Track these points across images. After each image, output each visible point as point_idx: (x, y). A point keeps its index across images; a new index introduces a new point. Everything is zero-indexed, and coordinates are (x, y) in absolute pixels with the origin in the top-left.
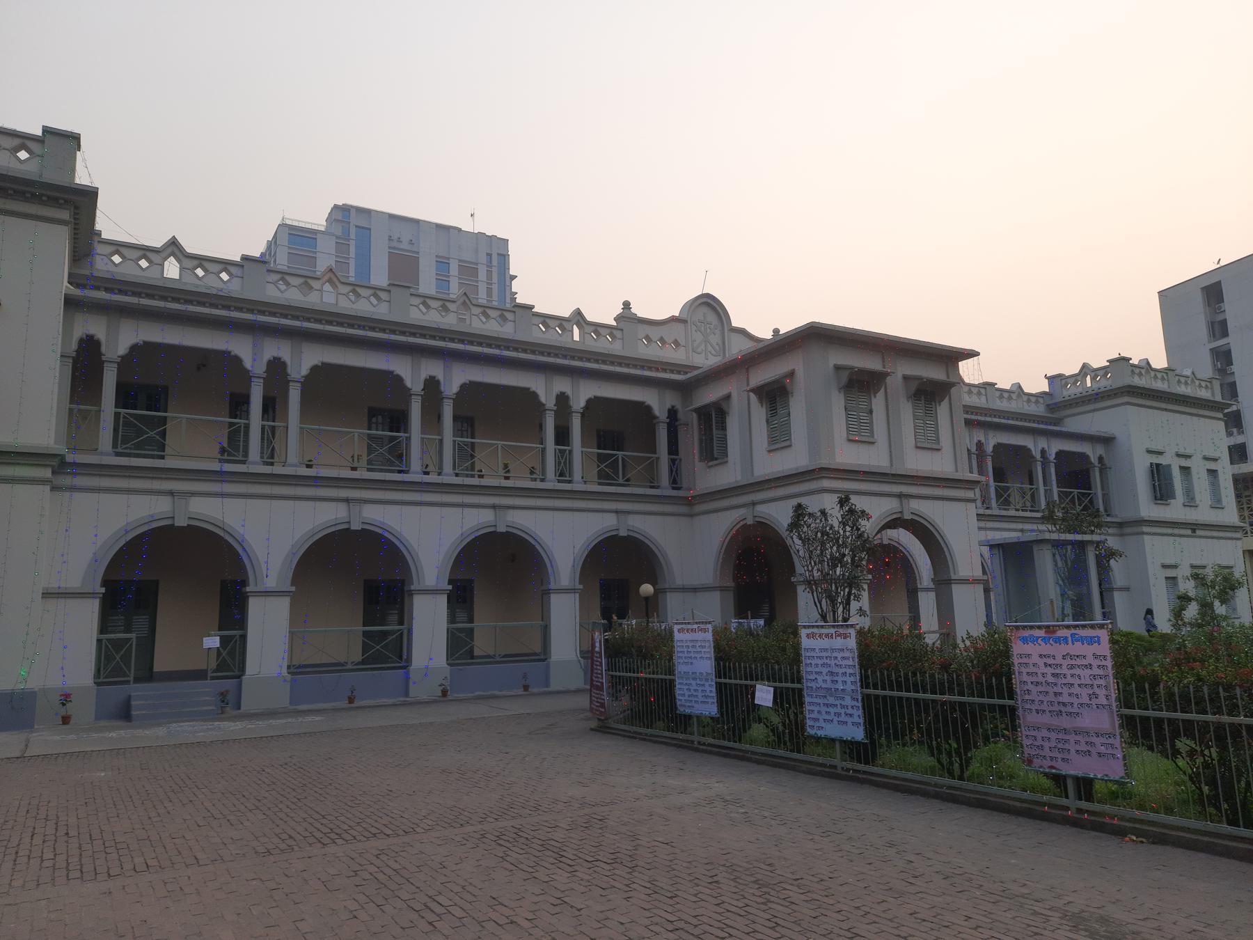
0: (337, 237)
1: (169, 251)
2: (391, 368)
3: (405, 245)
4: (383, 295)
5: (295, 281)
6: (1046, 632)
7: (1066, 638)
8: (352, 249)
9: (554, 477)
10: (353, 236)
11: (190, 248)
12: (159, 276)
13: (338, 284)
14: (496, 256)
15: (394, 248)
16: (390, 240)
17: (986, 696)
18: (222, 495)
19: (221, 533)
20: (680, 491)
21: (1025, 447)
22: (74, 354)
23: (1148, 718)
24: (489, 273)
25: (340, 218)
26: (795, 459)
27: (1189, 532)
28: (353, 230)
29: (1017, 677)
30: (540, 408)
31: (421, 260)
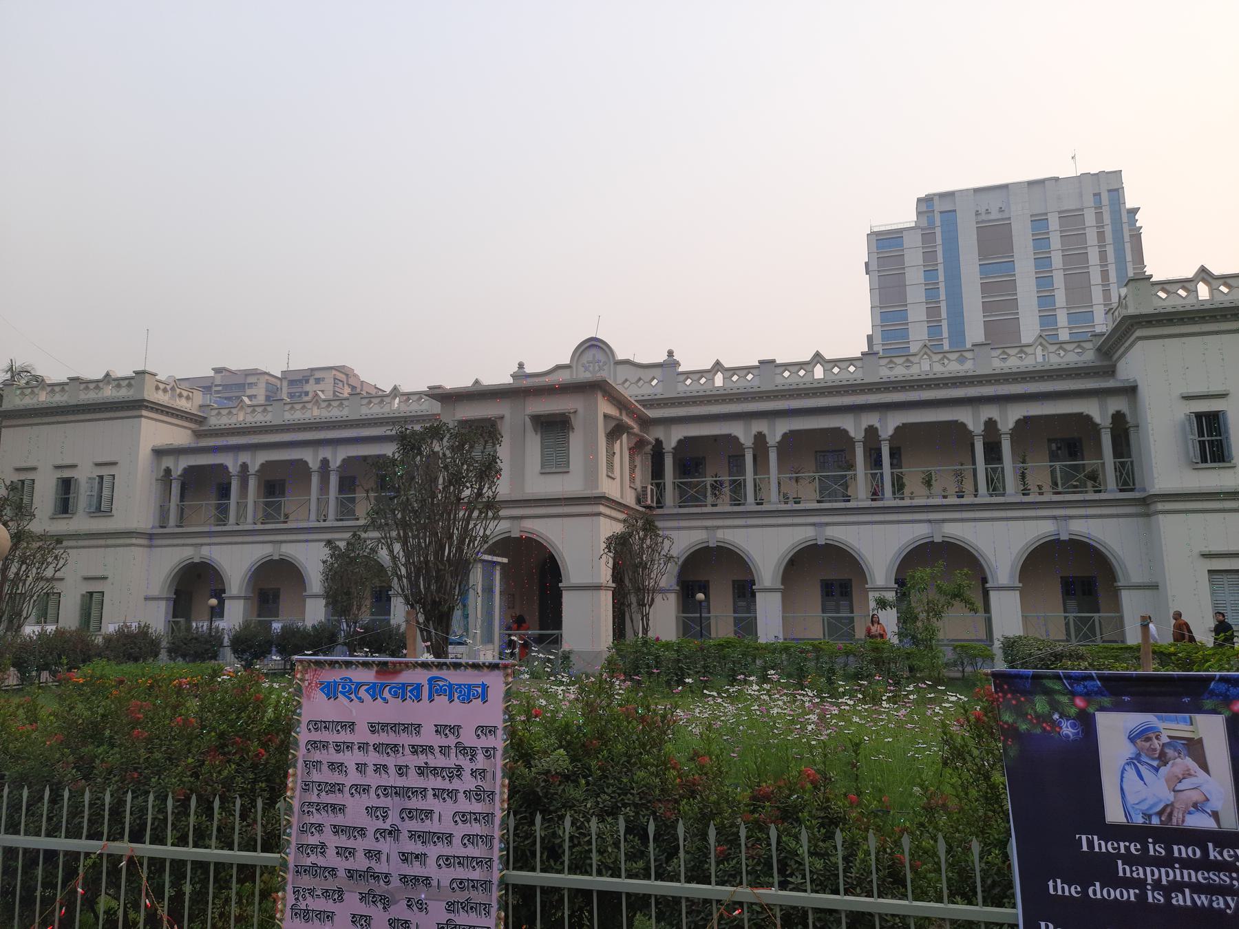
0: (922, 229)
2: (955, 419)
3: (995, 215)
6: (377, 672)
7: (419, 687)
8: (939, 240)
10: (938, 223)
11: (405, 388)
12: (711, 387)
14: (1106, 193)
15: (983, 221)
16: (976, 215)
17: (713, 879)
18: (1087, 517)
21: (222, 465)
23: (586, 894)
24: (1099, 215)
25: (925, 209)
28: (938, 217)
29: (299, 772)
30: (851, 442)
31: (1014, 227)
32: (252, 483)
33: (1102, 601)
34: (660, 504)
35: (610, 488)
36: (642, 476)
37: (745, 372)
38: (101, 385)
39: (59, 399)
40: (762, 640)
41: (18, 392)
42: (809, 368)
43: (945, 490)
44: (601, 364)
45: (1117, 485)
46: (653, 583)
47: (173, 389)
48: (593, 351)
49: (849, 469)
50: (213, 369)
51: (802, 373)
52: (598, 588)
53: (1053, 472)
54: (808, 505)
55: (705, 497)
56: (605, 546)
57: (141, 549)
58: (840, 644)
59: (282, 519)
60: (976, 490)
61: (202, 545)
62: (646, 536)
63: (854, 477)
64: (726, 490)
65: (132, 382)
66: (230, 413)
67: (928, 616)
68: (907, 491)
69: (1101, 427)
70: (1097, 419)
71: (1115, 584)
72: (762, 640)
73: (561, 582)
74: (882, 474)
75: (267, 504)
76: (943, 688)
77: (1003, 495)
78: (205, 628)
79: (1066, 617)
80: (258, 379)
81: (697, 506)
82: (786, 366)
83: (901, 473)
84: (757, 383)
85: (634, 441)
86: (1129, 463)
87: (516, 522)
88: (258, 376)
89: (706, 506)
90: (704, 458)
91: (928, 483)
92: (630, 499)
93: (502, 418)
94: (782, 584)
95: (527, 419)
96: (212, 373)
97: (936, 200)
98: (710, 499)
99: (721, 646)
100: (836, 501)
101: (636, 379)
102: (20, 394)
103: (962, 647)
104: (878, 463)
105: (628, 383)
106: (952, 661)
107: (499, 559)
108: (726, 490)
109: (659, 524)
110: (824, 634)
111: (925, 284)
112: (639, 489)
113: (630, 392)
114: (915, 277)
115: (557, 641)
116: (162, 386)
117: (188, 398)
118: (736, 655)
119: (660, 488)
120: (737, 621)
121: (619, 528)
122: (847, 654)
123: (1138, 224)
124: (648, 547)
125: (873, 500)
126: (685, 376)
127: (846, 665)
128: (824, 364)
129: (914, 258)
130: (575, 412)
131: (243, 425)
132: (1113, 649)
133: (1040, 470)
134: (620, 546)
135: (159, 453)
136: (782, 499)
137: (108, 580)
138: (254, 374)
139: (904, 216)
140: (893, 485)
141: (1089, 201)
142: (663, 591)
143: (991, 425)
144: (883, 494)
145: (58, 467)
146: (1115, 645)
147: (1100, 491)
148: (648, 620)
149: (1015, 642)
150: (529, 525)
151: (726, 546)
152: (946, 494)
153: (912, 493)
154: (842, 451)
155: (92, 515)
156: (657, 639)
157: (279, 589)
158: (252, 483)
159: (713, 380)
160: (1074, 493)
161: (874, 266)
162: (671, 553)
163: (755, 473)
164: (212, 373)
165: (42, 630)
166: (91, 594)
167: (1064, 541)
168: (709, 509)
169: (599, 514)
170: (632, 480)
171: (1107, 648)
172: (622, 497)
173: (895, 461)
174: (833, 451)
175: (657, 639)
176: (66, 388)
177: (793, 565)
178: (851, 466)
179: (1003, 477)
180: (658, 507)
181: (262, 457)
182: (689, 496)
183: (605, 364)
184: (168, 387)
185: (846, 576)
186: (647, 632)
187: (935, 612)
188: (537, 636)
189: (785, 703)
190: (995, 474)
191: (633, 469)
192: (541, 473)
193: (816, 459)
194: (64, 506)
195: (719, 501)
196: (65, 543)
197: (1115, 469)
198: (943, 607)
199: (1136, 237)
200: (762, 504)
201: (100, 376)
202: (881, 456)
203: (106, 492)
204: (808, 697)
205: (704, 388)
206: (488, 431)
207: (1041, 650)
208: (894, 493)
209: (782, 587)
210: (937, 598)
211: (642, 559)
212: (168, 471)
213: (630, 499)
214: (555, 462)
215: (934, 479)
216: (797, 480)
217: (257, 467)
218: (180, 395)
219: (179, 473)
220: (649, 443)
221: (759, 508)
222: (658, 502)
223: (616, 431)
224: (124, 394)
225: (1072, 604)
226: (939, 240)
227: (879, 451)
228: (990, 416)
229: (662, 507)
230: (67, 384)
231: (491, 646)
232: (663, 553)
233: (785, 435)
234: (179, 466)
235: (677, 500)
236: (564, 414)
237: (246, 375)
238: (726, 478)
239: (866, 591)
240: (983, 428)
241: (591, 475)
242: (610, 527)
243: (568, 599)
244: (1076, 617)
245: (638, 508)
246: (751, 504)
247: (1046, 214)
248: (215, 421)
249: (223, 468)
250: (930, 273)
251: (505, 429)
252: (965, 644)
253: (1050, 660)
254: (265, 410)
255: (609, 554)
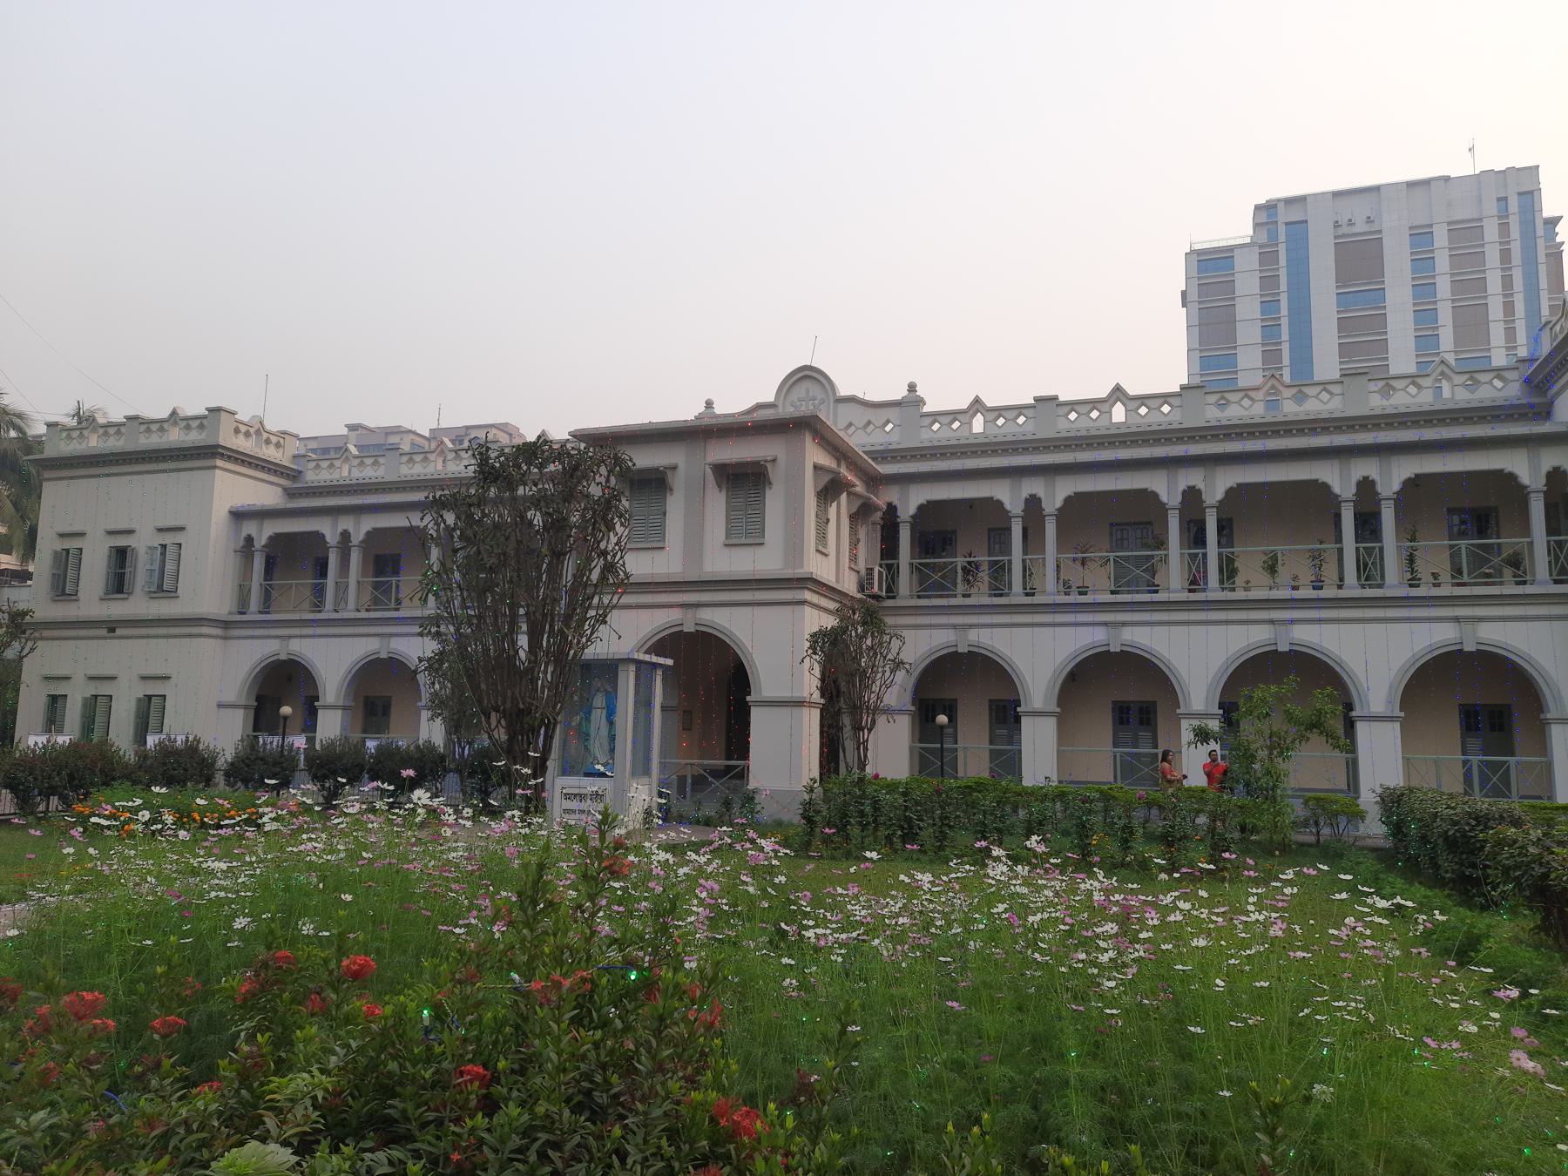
0: (1260, 247)
1: (1114, 397)
2: (1314, 477)
3: (1360, 227)
4: (1336, 389)
5: (418, 458)
8: (1283, 261)
9: (1548, 577)
10: (1282, 238)
11: (1132, 390)
13: (1453, 375)
15: (1344, 236)
19: (1148, 656)
20: (954, 599)
22: (1179, 506)
24: (1504, 228)
26: (766, 561)
27: (417, 629)
28: (1282, 229)
30: (1162, 509)
32: (355, 557)
33: (1520, 736)
34: (892, 592)
35: (822, 568)
36: (868, 554)
37: (1016, 412)
38: (166, 426)
39: (114, 444)
40: (1028, 781)
41: (64, 435)
42: (1105, 407)
43: (1295, 578)
44: (817, 402)
45: (1551, 575)
46: (875, 699)
47: (258, 432)
48: (807, 384)
49: (1158, 548)
50: (346, 426)
51: (1095, 414)
52: (799, 704)
53: (1454, 555)
54: (1096, 596)
55: (955, 585)
56: (808, 644)
57: (211, 640)
58: (1140, 791)
59: (393, 606)
60: (1341, 579)
61: (290, 637)
62: (865, 632)
63: (1165, 560)
64: (984, 575)
65: (205, 422)
66: (331, 466)
67: (1271, 754)
68: (1239, 580)
69: (1529, 490)
70: (1525, 478)
71: (1542, 716)
72: (1028, 781)
73: (749, 694)
74: (1205, 555)
75: (376, 586)
76: (1349, 877)
77: (1381, 586)
78: (275, 743)
79: (1465, 762)
80: (402, 439)
81: (941, 596)
82: (1073, 405)
83: (1233, 553)
84: (1030, 427)
85: (857, 504)
86: (1377, 549)
87: (690, 612)
88: (403, 435)
89: (955, 596)
90: (954, 532)
91: (1272, 569)
92: (849, 585)
93: (674, 468)
94: (1058, 706)
95: (709, 471)
96: (345, 431)
97: (1281, 207)
98: (961, 588)
99: (968, 790)
100: (1138, 592)
101: (864, 422)
102: (66, 437)
103: (1318, 799)
104: (1199, 539)
105: (853, 428)
106: (1302, 819)
107: (661, 660)
108: (984, 575)
109: (889, 621)
110: (1115, 777)
111: (1262, 320)
112: (863, 572)
113: (857, 441)
114: (1248, 309)
115: (742, 775)
116: (243, 429)
117: (278, 445)
118: (988, 801)
119: (892, 572)
120: (994, 755)
121: (830, 622)
122: (1150, 804)
123: (1558, 239)
124: (870, 648)
125: (1190, 591)
126: (931, 419)
127: (1147, 821)
128: (1126, 401)
129: (1247, 284)
130: (774, 460)
131: (348, 482)
132: (1545, 808)
133: (1435, 553)
134: (830, 646)
135: (238, 516)
136: (1061, 588)
137: (171, 681)
138: (397, 433)
139: (1237, 229)
140: (1221, 570)
141: (1491, 208)
142: (889, 711)
143: (1366, 486)
144: (1206, 583)
145: (111, 533)
146: (1538, 802)
147: (1525, 583)
148: (866, 749)
149: (1403, 795)
150: (706, 615)
151: (981, 651)
152: (1297, 584)
153: (1248, 582)
154: (1150, 523)
155: (154, 595)
156: (876, 776)
157: (956, 700)
158: (355, 557)
159: (970, 424)
160: (1486, 584)
161: (1193, 296)
162: (902, 656)
163: (1025, 552)
164: (345, 431)
165: (49, 741)
166: (149, 697)
167: (1471, 653)
168: (958, 601)
169: (803, 602)
170: (854, 558)
171: (1534, 807)
172: (837, 581)
173: (1224, 540)
174: (1135, 524)
175: (876, 776)
176: (123, 429)
177: (1074, 680)
178: (1161, 543)
179: (1382, 559)
180: (889, 598)
181: (369, 523)
182: (932, 583)
183: (822, 402)
184: (252, 430)
185: (1148, 697)
186: (865, 766)
187: (1278, 746)
188: (723, 768)
189: (1057, 894)
190: (1370, 556)
191: (854, 544)
192: (726, 545)
193: (1111, 534)
194: (118, 584)
195: (973, 591)
196: (119, 632)
197: (1549, 551)
198: (1293, 742)
199: (1556, 256)
200: (1033, 594)
201: (165, 414)
202: (1205, 530)
203: (170, 567)
204: (1095, 885)
205: (957, 434)
206: (655, 483)
207: (1452, 808)
208: (1221, 582)
209: (1058, 710)
210: (1285, 729)
211: (860, 665)
212: (249, 540)
213: (849, 585)
214: (745, 530)
215: (1280, 562)
216: (1083, 562)
217: (361, 537)
218: (268, 442)
219: (263, 543)
220: (877, 508)
221: (1029, 600)
222: (889, 590)
223: (830, 490)
224: (195, 438)
225: (1474, 743)
226: (1283, 261)
227: (1376, 515)
228: (1366, 474)
229: (894, 598)
230: (123, 424)
231: (646, 780)
232: (890, 656)
233: (1068, 500)
234: (263, 533)
235: (916, 588)
236: (758, 462)
237: (387, 434)
238: (983, 559)
239: (1176, 720)
240: (1354, 491)
241: (794, 549)
242: (817, 619)
243: (757, 716)
244: (1482, 762)
245: (859, 596)
246: (1017, 595)
247: (1431, 226)
248: (313, 477)
249: (318, 537)
250: (1269, 305)
251: (678, 482)
252: (1322, 795)
253: (1468, 824)
254: (376, 463)
255: (814, 656)
